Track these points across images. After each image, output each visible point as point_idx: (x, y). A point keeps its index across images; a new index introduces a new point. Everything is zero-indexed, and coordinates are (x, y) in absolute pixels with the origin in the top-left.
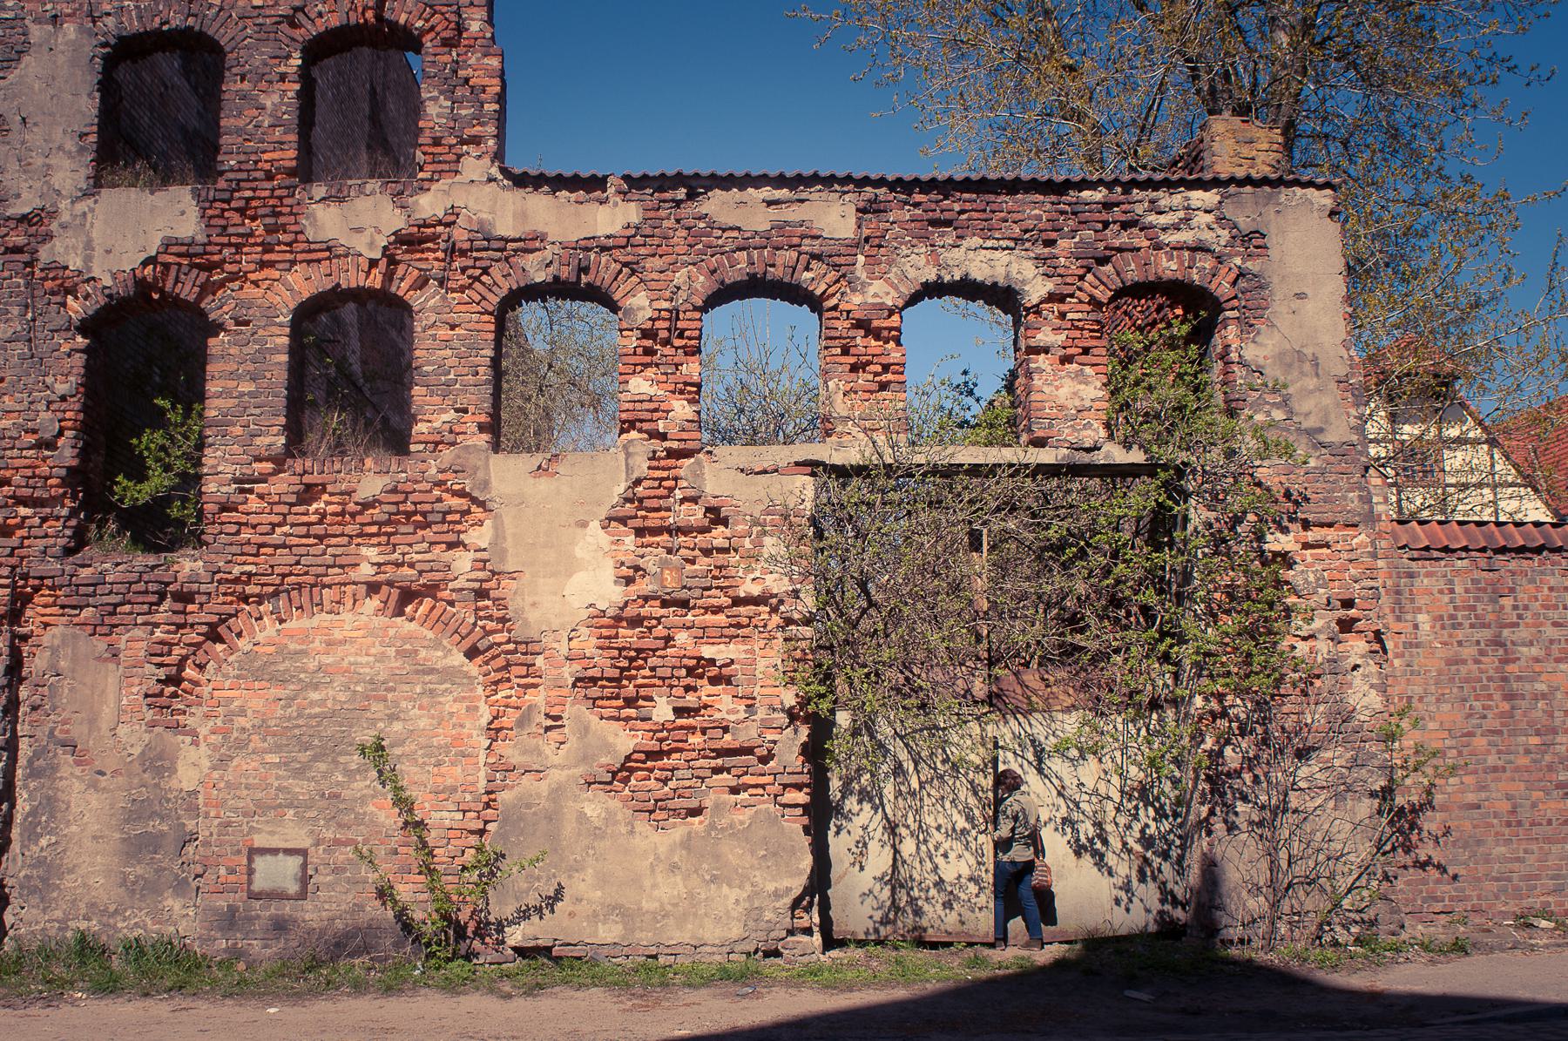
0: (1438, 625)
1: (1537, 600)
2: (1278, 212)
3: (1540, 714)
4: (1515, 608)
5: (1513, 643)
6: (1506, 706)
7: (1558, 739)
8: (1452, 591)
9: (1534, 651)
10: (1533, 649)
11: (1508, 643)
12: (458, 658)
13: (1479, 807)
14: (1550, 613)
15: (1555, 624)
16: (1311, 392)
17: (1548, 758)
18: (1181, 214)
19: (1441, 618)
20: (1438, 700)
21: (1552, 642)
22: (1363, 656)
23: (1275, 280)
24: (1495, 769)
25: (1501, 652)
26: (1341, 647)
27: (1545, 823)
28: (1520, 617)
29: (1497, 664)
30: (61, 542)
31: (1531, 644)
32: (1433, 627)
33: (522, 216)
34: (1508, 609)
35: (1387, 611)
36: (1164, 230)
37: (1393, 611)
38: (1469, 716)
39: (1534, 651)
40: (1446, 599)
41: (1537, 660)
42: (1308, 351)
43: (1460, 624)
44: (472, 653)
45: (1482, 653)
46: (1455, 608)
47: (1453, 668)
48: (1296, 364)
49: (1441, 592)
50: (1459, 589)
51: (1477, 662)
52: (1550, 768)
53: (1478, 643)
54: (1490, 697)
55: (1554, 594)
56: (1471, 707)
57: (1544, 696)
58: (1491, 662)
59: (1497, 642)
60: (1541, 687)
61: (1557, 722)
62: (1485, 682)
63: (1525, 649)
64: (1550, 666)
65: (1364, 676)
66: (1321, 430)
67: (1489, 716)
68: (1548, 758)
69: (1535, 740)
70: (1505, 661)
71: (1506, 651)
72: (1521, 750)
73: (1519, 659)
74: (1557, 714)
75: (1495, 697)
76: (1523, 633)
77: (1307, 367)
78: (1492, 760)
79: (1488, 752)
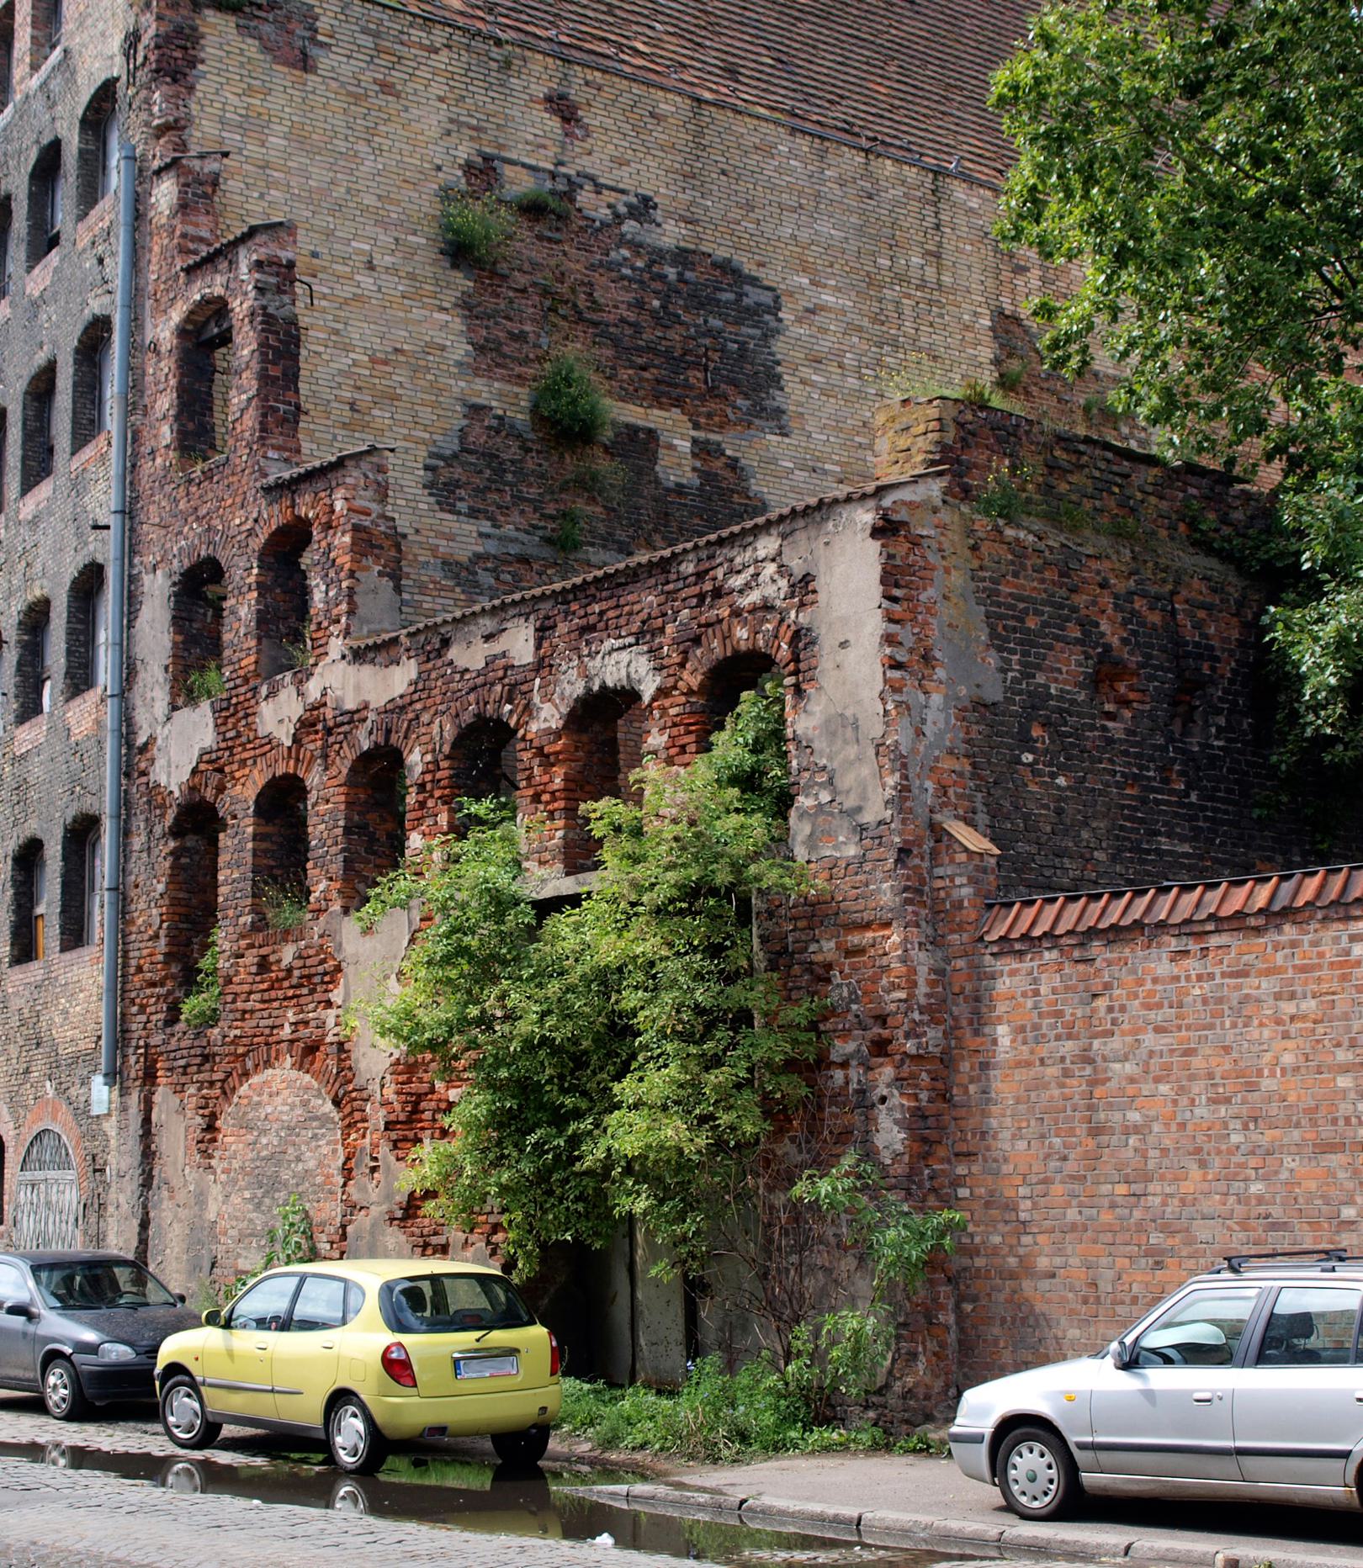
0: (1020, 1038)
1: (1136, 996)
2: (827, 544)
3: (1131, 1153)
4: (1110, 1009)
5: (1105, 1059)
6: (1091, 1143)
7: (1151, 1188)
8: (1036, 993)
9: (1129, 1068)
10: (1127, 1065)
11: (1099, 1059)
12: (329, 1106)
13: (1053, 1276)
14: (1152, 1015)
15: (1159, 1030)
16: (852, 763)
17: (1137, 1214)
18: (751, 570)
19: (1022, 1029)
20: (1014, 1136)
21: (1151, 1054)
22: (888, 1086)
23: (823, 631)
24: (1074, 1227)
25: (1088, 1071)
26: (870, 1075)
27: (1128, 1300)
28: (1114, 1022)
29: (1084, 1087)
30: (161, 1016)
31: (1125, 1059)
32: (1013, 1041)
33: (358, 688)
34: (1102, 1013)
35: (964, 1023)
36: (741, 592)
37: (971, 1023)
38: (1047, 1157)
39: (1129, 1068)
40: (1030, 1003)
41: (1132, 1080)
42: (849, 713)
43: (1044, 1036)
44: (337, 1102)
45: (1066, 1073)
46: (1040, 1015)
47: (1033, 1094)
48: (840, 730)
49: (1024, 994)
50: (1044, 990)
51: (1062, 1086)
52: (1140, 1228)
53: (1063, 1059)
54: (1071, 1132)
55: (1159, 987)
56: (1050, 1146)
57: (1137, 1129)
58: (1076, 1087)
59: (1086, 1059)
60: (1134, 1117)
61: (1151, 1165)
62: (1069, 1112)
63: (1117, 1066)
64: (1146, 1089)
65: (888, 1109)
66: (859, 809)
67: (1072, 1156)
68: (1137, 1214)
69: (1122, 1189)
70: (1093, 1082)
71: (1095, 1069)
72: (1106, 1202)
73: (1109, 1079)
74: (1152, 1153)
75: (1078, 1132)
76: (1116, 1043)
77: (849, 732)
78: (1072, 1214)
79: (1068, 1205)
